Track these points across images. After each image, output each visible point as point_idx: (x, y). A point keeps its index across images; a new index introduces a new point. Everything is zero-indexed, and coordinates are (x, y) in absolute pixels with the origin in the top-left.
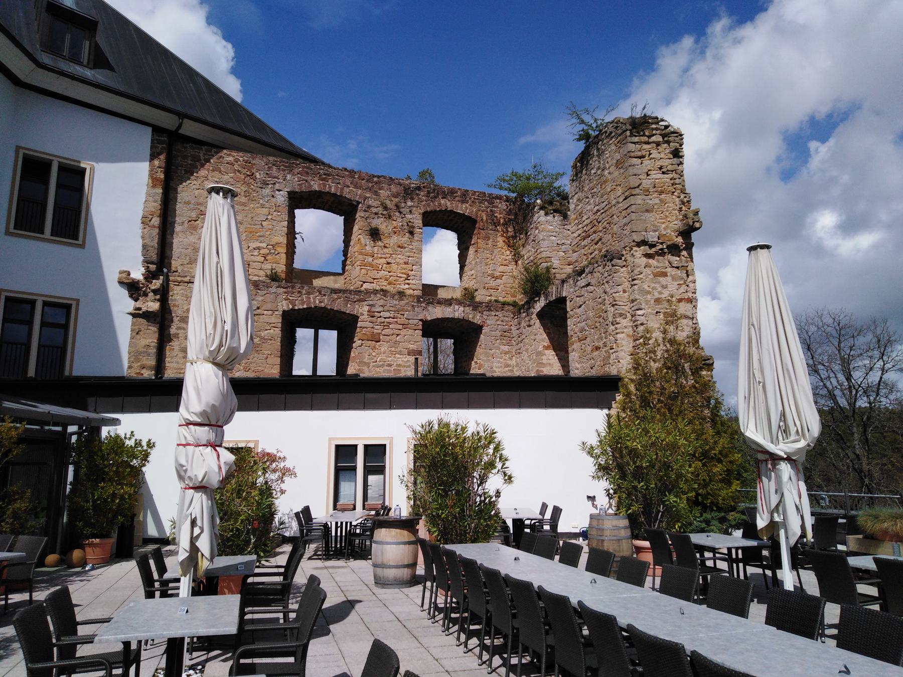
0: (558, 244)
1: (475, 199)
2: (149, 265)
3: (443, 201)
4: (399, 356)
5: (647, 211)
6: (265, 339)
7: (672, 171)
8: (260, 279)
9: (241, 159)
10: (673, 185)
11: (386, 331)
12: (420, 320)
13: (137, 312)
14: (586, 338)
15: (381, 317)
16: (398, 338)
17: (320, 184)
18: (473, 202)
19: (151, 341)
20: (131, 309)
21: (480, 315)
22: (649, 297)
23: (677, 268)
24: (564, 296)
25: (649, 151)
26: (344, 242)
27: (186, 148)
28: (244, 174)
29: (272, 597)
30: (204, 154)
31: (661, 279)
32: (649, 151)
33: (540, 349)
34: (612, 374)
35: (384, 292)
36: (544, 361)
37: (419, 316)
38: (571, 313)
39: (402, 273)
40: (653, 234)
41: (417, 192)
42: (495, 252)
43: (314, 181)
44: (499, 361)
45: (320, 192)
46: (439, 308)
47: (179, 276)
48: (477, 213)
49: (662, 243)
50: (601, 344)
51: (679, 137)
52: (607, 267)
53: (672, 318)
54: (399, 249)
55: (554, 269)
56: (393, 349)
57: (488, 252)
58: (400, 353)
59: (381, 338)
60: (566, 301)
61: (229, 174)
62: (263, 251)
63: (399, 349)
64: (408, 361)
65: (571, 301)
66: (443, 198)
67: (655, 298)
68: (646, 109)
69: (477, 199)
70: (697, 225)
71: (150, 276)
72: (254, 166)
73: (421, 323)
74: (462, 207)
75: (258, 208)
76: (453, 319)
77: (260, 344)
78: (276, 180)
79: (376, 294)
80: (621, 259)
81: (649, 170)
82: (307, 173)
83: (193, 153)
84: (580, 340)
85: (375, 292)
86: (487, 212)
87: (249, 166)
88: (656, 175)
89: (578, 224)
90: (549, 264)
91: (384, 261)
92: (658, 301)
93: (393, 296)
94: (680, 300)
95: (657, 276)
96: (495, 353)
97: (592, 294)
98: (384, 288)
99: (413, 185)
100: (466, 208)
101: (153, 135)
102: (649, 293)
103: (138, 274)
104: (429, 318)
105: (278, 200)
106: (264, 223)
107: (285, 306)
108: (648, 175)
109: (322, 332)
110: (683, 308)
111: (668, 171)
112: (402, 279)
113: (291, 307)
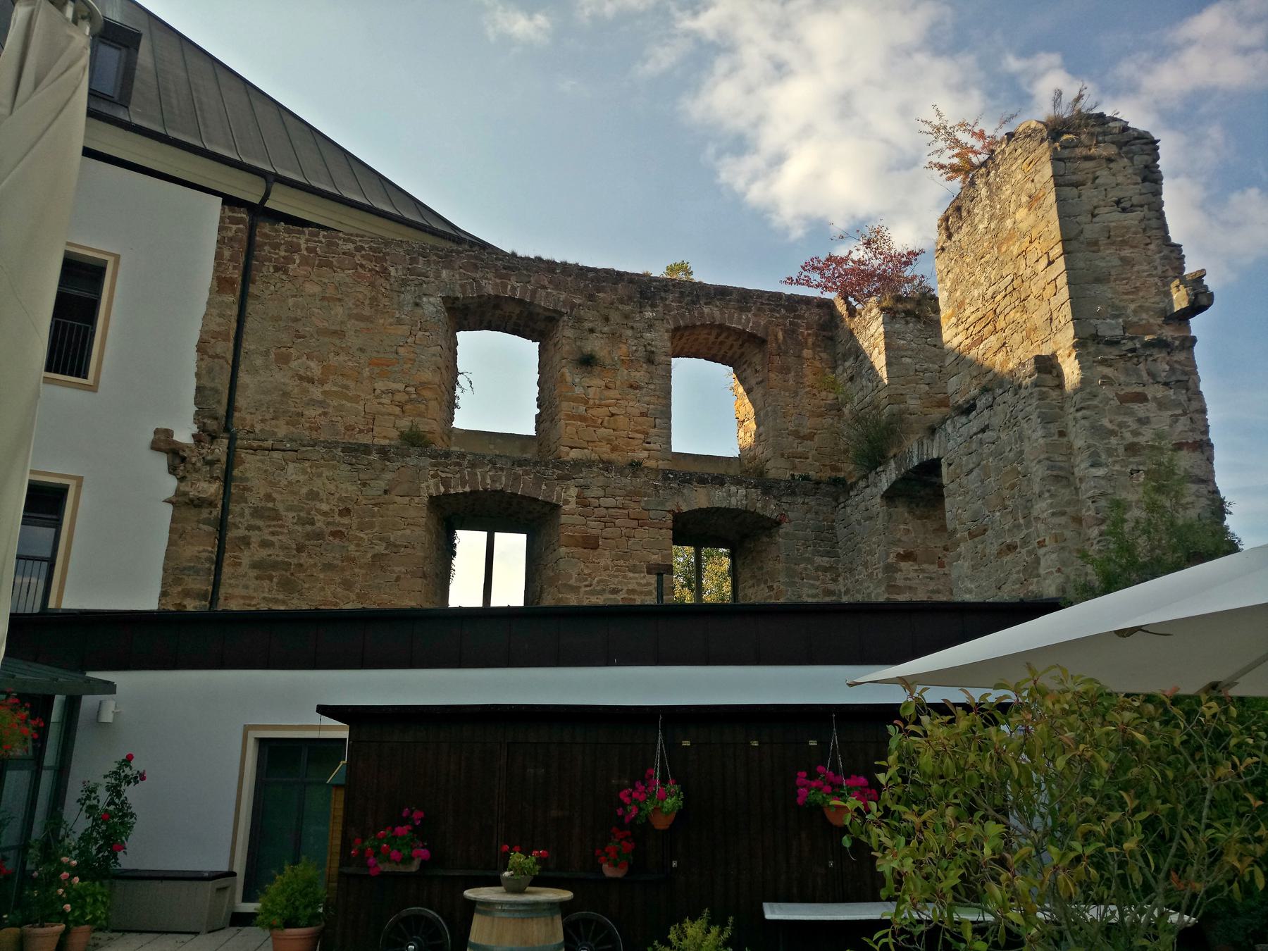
0: (916, 371)
1: (762, 304)
2: (206, 420)
3: (706, 310)
4: (631, 575)
5: (1098, 280)
6: (396, 546)
7: (1142, 206)
8: (393, 443)
9: (366, 246)
10: (1144, 230)
11: (609, 531)
12: (669, 512)
13: (180, 499)
14: (985, 530)
15: (600, 506)
16: (630, 543)
17: (496, 284)
18: (759, 309)
19: (201, 548)
20: (170, 493)
21: (775, 502)
22: (1114, 441)
23: (1166, 384)
24: (935, 456)
25: (1094, 172)
26: (539, 384)
27: (335, 305)
28: (370, 270)
29: (593, 928)
30: (307, 241)
31: (1135, 406)
32: (1094, 172)
33: (890, 560)
34: (1044, 597)
35: (607, 465)
36: (900, 583)
37: (667, 504)
38: (951, 486)
39: (637, 431)
40: (1113, 322)
41: (663, 294)
42: (800, 393)
43: (487, 279)
44: (813, 585)
45: (497, 297)
46: (701, 489)
47: (254, 439)
48: (766, 327)
49: (1132, 339)
50: (1017, 540)
51: (1151, 146)
52: (1022, 390)
53: (1163, 481)
54: (631, 390)
55: (911, 414)
56: (621, 562)
57: (787, 394)
58: (634, 569)
59: (600, 543)
60: (940, 466)
61: (346, 271)
62: (401, 397)
63: (632, 562)
64: (648, 584)
65: (950, 465)
66: (706, 304)
67: (1126, 442)
68: (1082, 101)
69: (768, 304)
70: (1203, 300)
71: (204, 436)
72: (387, 258)
73: (670, 516)
74: (741, 319)
75: (391, 324)
76: (727, 511)
77: (386, 554)
78: (423, 278)
79: (590, 467)
80: (1050, 373)
81: (1095, 208)
82: (476, 267)
83: (290, 239)
84: (972, 535)
85: (589, 464)
86: (785, 325)
87: (379, 257)
88: (1113, 217)
89: (957, 325)
90: (902, 406)
91: (603, 411)
92: (1132, 449)
93: (621, 471)
94: (1179, 447)
95: (1127, 401)
96: (805, 569)
97: (994, 446)
98: (605, 457)
99: (654, 284)
100: (748, 321)
101: (223, 209)
102: (1112, 433)
103: (184, 435)
104: (685, 509)
105: (426, 312)
106: (401, 350)
107: (431, 487)
108: (1094, 216)
109: (499, 537)
110: (1185, 461)
111: (1132, 206)
112: (636, 442)
113: (442, 489)
